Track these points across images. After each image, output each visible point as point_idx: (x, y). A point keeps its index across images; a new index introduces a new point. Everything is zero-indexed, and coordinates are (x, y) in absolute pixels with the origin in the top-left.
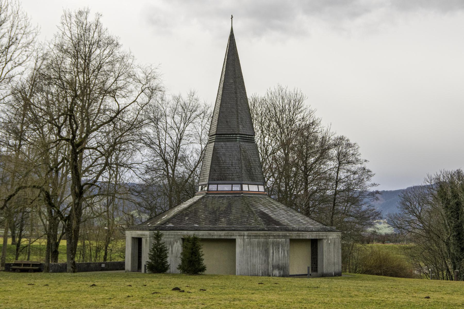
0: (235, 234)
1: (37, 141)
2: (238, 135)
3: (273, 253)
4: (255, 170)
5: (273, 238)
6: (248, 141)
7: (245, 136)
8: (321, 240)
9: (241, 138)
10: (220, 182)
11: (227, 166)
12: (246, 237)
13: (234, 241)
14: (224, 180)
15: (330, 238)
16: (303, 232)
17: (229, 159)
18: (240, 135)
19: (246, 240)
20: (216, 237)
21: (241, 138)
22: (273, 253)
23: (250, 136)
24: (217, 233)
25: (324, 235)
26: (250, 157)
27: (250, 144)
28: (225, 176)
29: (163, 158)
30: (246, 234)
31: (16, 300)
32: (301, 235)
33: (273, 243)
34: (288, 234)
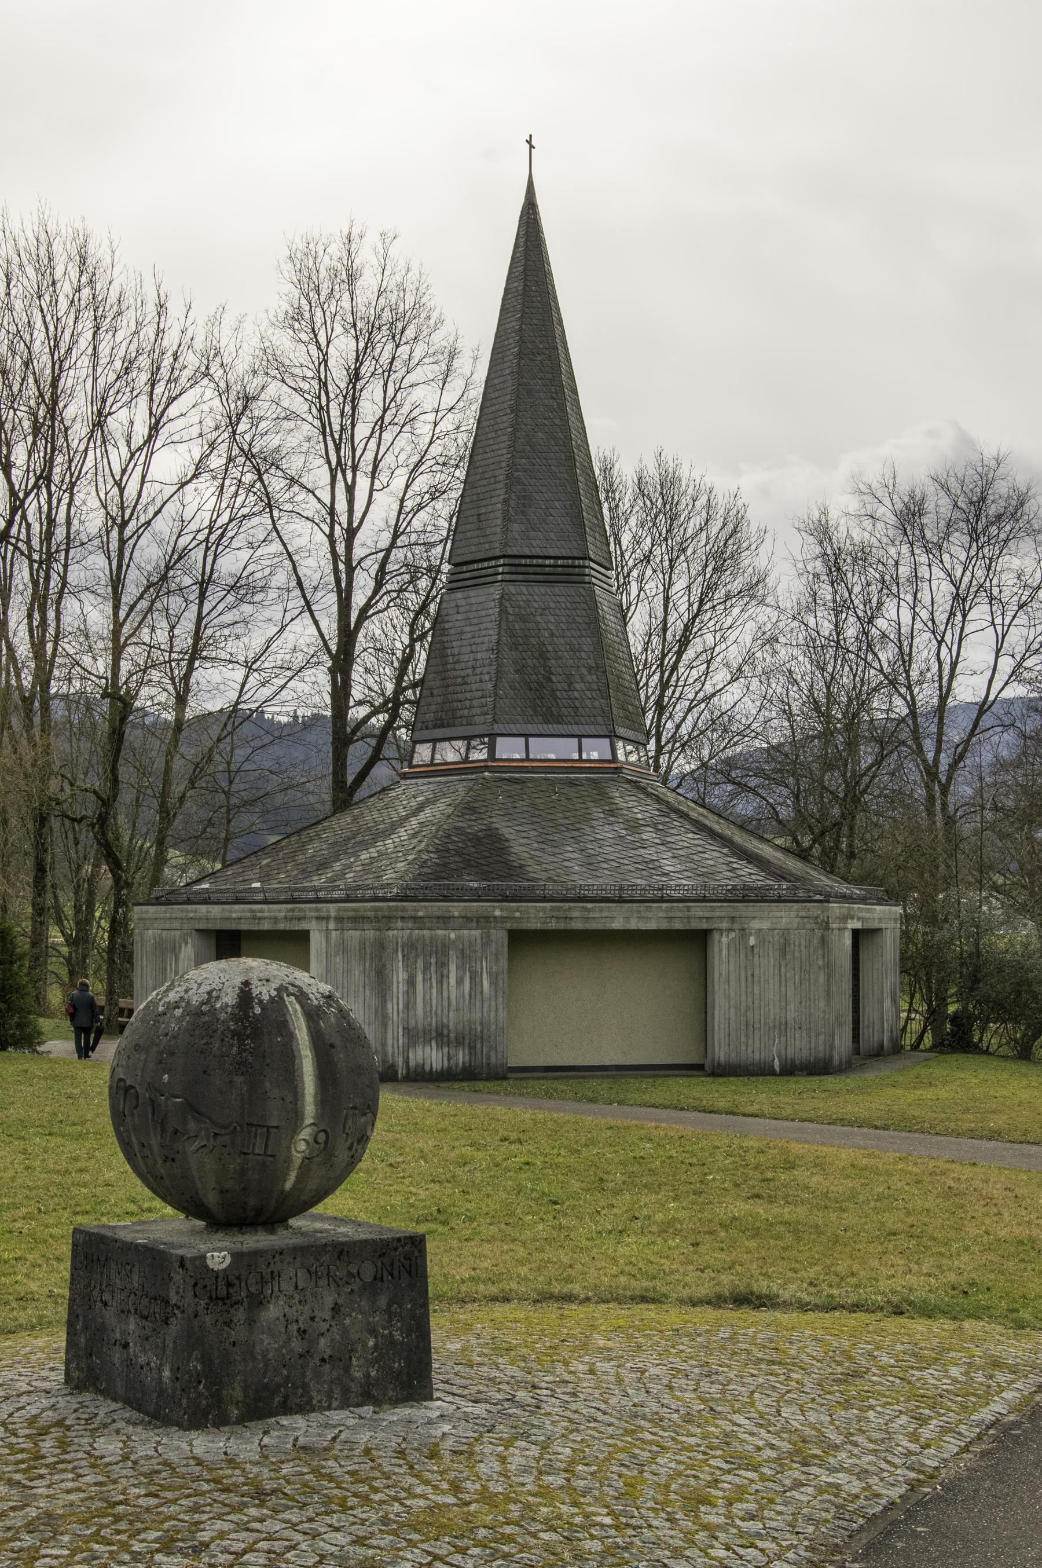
0: (308, 914)
2: (501, 562)
3: (411, 982)
4: (570, 684)
5: (410, 925)
6: (551, 578)
7: (528, 561)
9: (513, 569)
10: (439, 733)
11: (462, 673)
12: (332, 925)
13: (303, 937)
14: (449, 726)
15: (755, 925)
16: (590, 905)
17: (469, 649)
18: (507, 561)
19: (334, 933)
20: (266, 926)
21: (513, 569)
22: (411, 982)
23: (535, 561)
24: (270, 911)
25: (717, 914)
26: (552, 635)
27: (571, 589)
28: (454, 710)
29: (941, 696)
30: (333, 914)
32: (576, 914)
33: (411, 948)
34: (497, 913)
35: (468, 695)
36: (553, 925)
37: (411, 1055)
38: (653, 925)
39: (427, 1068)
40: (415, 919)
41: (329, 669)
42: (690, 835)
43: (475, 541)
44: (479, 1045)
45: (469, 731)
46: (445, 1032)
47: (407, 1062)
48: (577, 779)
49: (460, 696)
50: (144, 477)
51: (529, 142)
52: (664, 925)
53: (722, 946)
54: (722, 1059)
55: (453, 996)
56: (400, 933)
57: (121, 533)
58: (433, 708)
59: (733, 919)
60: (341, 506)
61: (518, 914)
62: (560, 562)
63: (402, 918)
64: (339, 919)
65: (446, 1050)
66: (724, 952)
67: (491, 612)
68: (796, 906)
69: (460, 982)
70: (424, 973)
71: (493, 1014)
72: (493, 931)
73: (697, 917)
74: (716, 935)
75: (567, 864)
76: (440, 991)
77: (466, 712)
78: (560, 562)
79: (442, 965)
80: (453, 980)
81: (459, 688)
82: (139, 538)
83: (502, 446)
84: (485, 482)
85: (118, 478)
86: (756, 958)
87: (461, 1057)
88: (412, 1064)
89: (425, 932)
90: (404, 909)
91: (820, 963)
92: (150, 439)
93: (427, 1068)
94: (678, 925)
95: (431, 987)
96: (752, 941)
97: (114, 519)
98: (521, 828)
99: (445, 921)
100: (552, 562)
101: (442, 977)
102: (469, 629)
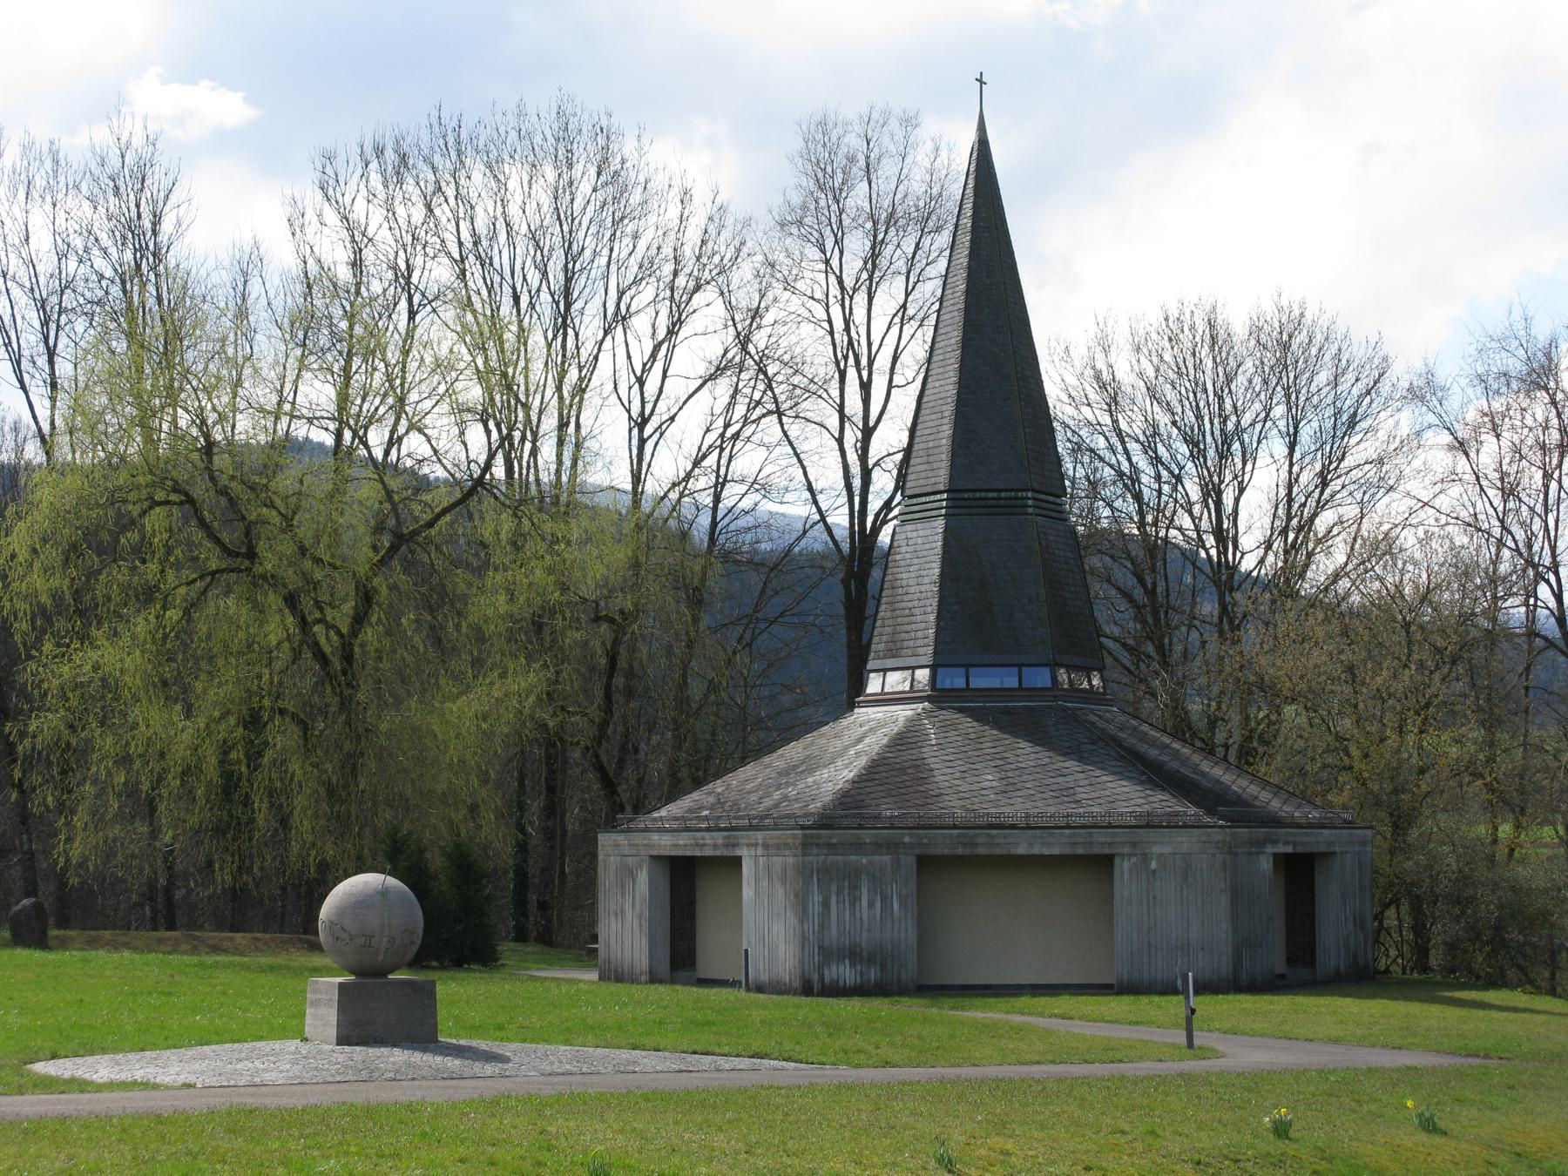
1: (168, 560)
3: (826, 904)
5: (825, 851)
6: (993, 510)
7: (983, 494)
8: (1327, 855)
10: (889, 663)
11: (910, 605)
13: (737, 862)
15: (1157, 849)
16: (994, 832)
22: (826, 904)
23: (978, 495)
25: (1119, 840)
31: (1518, 1149)
34: (907, 840)
35: (914, 626)
36: (960, 851)
37: (826, 972)
38: (1056, 851)
39: (841, 984)
40: (829, 845)
41: (842, 581)
42: (1113, 763)
43: (923, 475)
44: (890, 963)
45: (912, 661)
46: (858, 951)
47: (822, 978)
48: (1014, 707)
49: (907, 628)
50: (665, 372)
51: (981, 82)
52: (1067, 851)
53: (1123, 867)
54: (1125, 979)
55: (865, 917)
56: (815, 859)
57: (641, 431)
58: (884, 638)
59: (1134, 844)
60: (854, 404)
61: (925, 841)
62: (1003, 495)
63: (817, 845)
64: (766, 846)
65: (858, 968)
66: (1126, 876)
67: (934, 545)
68: (1196, 831)
69: (871, 904)
70: (837, 896)
71: (902, 934)
72: (902, 857)
73: (1100, 843)
74: (1117, 860)
75: (983, 792)
76: (853, 913)
77: (911, 643)
78: (1003, 495)
79: (855, 888)
80: (865, 903)
81: (905, 620)
82: (662, 434)
83: (948, 381)
84: (934, 417)
85: (639, 374)
86: (1158, 882)
87: (873, 974)
88: (827, 980)
89: (839, 857)
90: (819, 836)
91: (1223, 886)
92: (672, 332)
93: (841, 984)
94: (1080, 851)
95: (845, 909)
96: (1154, 865)
97: (636, 422)
98: (947, 758)
99: (857, 847)
100: (995, 494)
101: (855, 900)
102: (916, 561)
